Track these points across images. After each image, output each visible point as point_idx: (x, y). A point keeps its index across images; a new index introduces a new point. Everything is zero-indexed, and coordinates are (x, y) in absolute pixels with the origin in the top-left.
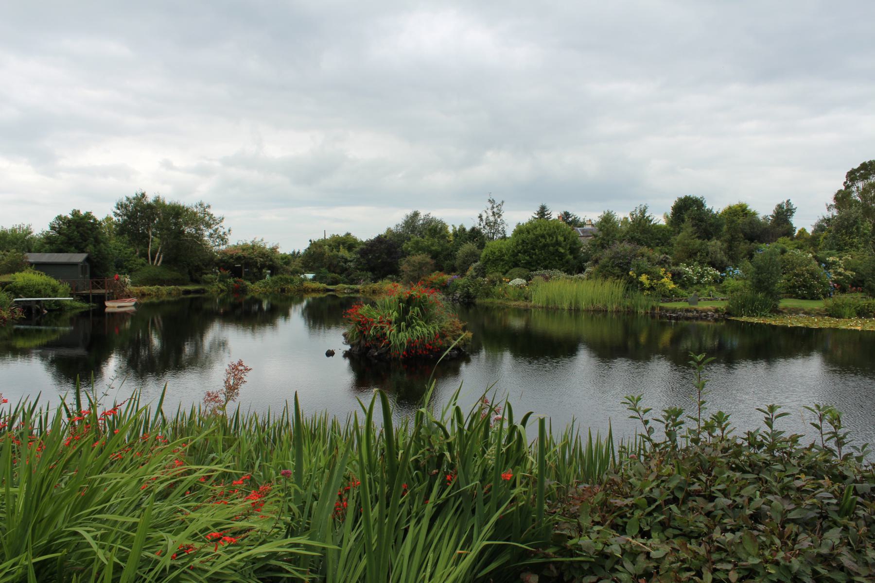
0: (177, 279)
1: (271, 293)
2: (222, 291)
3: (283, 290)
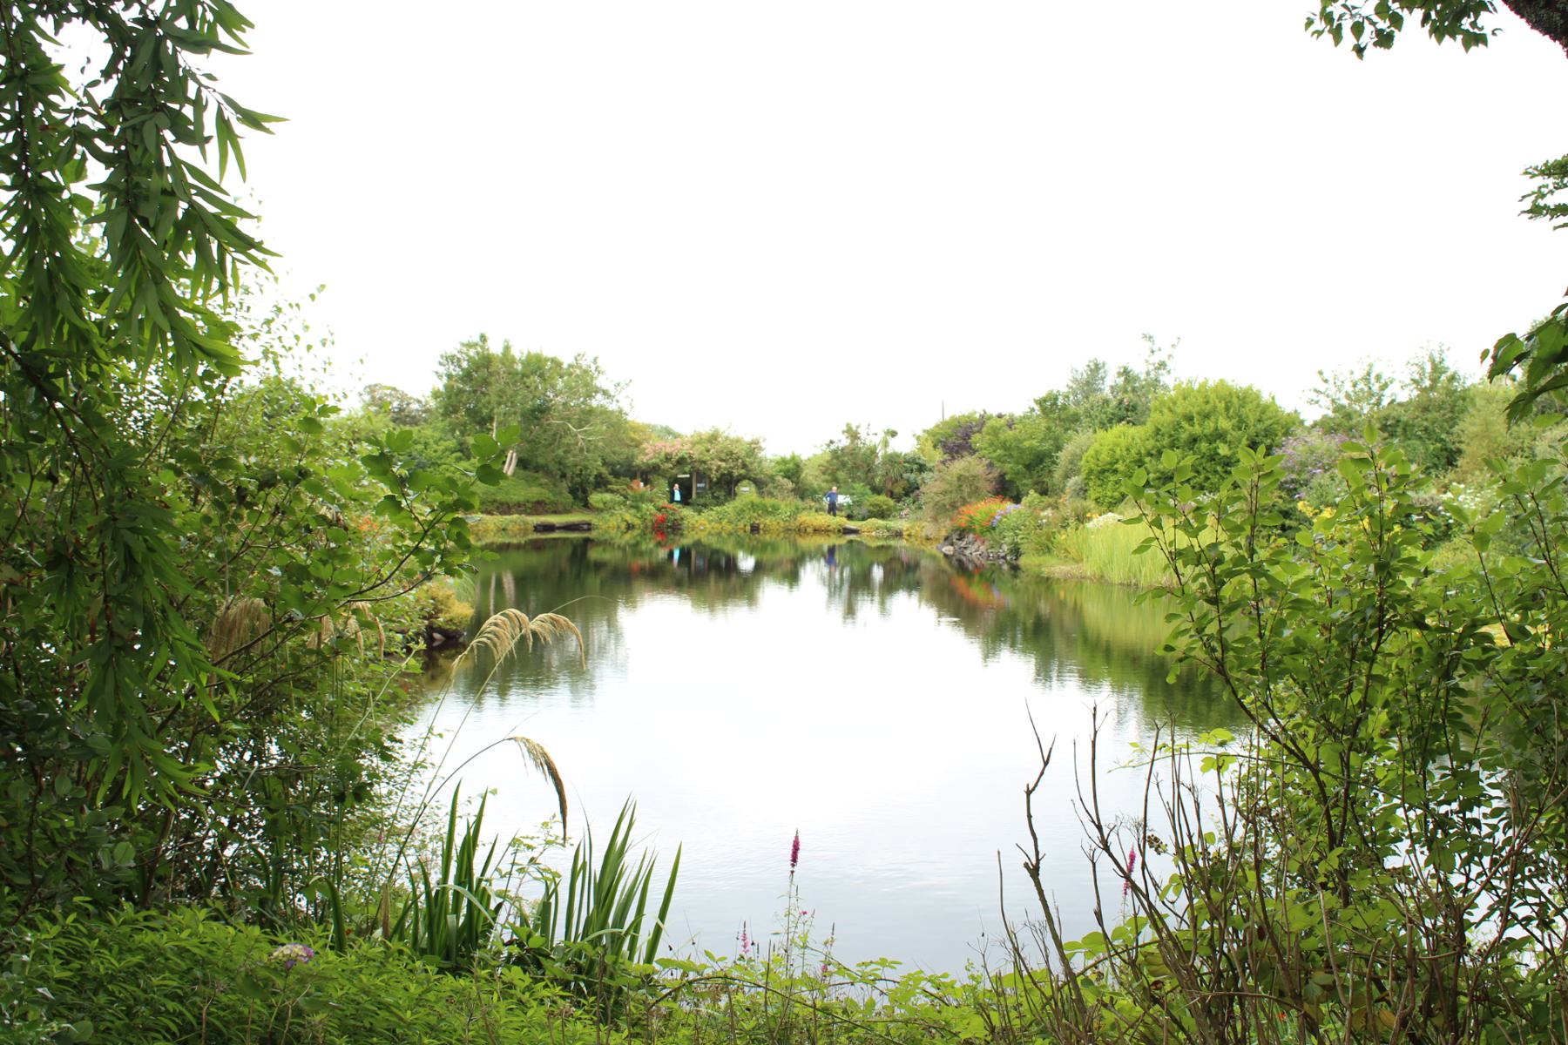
0: (539, 503)
1: (730, 534)
2: (630, 527)
3: (755, 529)
